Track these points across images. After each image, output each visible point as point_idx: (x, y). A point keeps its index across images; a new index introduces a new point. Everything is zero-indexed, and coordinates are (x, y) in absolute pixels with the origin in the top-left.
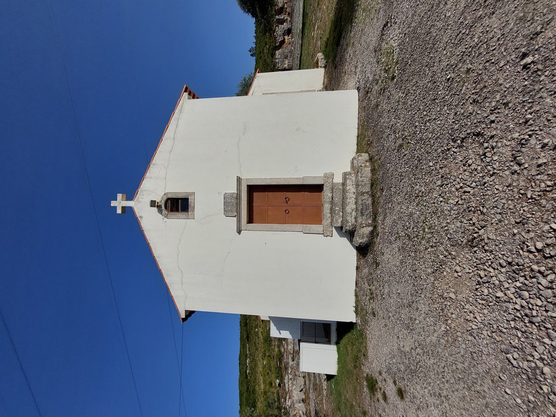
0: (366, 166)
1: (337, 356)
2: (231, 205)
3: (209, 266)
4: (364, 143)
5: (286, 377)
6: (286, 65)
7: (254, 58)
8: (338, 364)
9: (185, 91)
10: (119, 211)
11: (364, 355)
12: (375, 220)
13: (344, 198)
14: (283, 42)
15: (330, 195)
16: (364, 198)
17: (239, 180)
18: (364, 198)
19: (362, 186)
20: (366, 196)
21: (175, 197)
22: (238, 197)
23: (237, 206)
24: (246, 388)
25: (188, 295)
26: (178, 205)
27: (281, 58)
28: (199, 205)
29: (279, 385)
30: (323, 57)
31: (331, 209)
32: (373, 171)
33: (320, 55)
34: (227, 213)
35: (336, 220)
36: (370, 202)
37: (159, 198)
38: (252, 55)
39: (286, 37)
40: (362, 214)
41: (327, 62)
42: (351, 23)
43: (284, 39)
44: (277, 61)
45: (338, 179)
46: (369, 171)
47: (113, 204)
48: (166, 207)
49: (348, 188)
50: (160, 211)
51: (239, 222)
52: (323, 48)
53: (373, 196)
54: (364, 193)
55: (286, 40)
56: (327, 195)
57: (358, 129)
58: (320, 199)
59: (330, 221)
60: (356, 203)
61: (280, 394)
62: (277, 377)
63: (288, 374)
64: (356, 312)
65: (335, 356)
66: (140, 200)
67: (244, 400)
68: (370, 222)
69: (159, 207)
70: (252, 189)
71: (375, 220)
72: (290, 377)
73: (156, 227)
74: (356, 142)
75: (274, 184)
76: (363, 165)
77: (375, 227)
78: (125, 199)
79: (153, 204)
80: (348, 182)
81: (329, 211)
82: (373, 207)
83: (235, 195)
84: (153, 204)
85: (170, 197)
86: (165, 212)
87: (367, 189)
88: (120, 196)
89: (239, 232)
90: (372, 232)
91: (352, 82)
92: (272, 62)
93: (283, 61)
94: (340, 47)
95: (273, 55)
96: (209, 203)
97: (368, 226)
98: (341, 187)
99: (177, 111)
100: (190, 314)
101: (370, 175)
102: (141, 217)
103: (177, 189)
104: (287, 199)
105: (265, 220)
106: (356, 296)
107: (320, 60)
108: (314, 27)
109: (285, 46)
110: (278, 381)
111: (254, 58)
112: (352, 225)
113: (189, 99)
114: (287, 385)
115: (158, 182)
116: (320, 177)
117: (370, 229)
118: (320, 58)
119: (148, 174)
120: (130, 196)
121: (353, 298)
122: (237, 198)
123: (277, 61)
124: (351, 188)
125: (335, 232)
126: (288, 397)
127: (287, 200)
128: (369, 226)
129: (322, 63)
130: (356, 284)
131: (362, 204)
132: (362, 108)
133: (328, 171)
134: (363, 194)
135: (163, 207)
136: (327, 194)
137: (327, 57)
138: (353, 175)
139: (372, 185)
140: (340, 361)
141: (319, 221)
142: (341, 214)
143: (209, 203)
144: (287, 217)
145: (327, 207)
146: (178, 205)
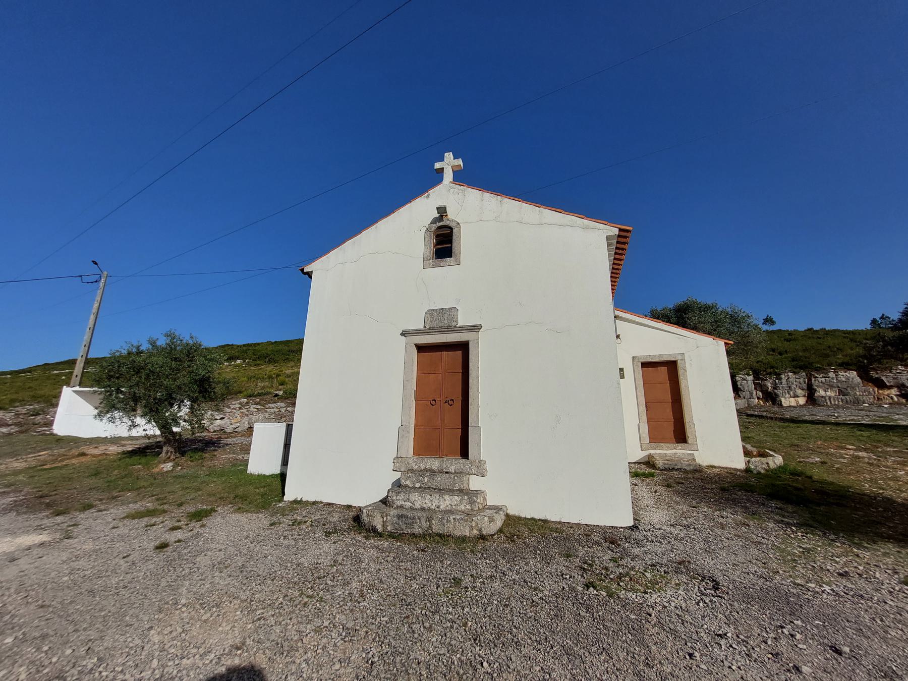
0: (472, 528)
1: (267, 474)
2: (441, 319)
3: (364, 296)
4: (514, 527)
5: (283, 405)
6: (821, 392)
7: (869, 327)
8: (259, 475)
9: (620, 230)
10: (437, 165)
11: (240, 508)
12: (391, 535)
13: (440, 491)
14: (881, 385)
15: (452, 469)
16: (423, 521)
17: (476, 328)
18: (423, 521)
19: (441, 520)
20: (426, 525)
21: (454, 237)
22: (451, 329)
23: (438, 328)
24: (293, 349)
25: (332, 273)
26: (444, 243)
27: (838, 381)
28: (446, 271)
29: (276, 395)
30: (772, 466)
31: (431, 470)
32: (463, 539)
33: (776, 460)
34: (430, 313)
35: (409, 477)
36: (417, 530)
37: (452, 215)
38: (874, 322)
39: (894, 392)
40: (400, 517)
41: (759, 473)
42: (799, 525)
43: (890, 387)
44: (831, 374)
45: (475, 483)
46: (464, 534)
47: (449, 156)
48: (440, 228)
49: (447, 497)
50: (434, 221)
51: (417, 332)
52: (792, 465)
53: (423, 536)
54: (430, 522)
55: (886, 392)
56: (451, 465)
57: (560, 523)
58: (450, 453)
59: (415, 467)
60: (423, 509)
61: (265, 397)
62: (285, 392)
63: (287, 407)
64: (295, 502)
65: (268, 472)
66: (452, 191)
67: (280, 347)
68: (389, 528)
69: (441, 218)
70: (464, 347)
71: (391, 535)
72: (283, 410)
73: (412, 220)
74: (537, 517)
75: (470, 381)
76: (474, 524)
77: (380, 535)
78: (455, 169)
79: (442, 211)
80: (456, 498)
81: (428, 467)
82: (410, 535)
83: (454, 324)
84: (442, 211)
85: (454, 231)
86: (434, 227)
87: (436, 528)
88: (460, 162)
89: (403, 334)
90: (374, 530)
91: (658, 517)
92: (830, 365)
93: (831, 387)
94: (760, 499)
95: (846, 366)
96: (446, 286)
97: (384, 524)
98: (457, 487)
99: (586, 222)
100: (310, 275)
101: (457, 533)
102: (428, 196)
103: (464, 242)
104: (451, 402)
105: (422, 370)
106: (315, 503)
107: (764, 460)
108: (865, 450)
109: (871, 388)
110: (281, 393)
111: (869, 327)
112: (393, 501)
113: (608, 238)
114: (273, 405)
115: (477, 212)
116: (480, 454)
117: (380, 528)
118: (770, 460)
119: (487, 195)
120: (460, 177)
121: (312, 499)
122: (449, 327)
123: (831, 374)
124: (447, 502)
125: (398, 475)
126: (259, 407)
127: (450, 402)
128: (383, 526)
129: (759, 464)
130: (329, 504)
131: (414, 518)
132: (587, 533)
133: (488, 467)
134: (429, 519)
135: (441, 224)
136: (454, 464)
137: (772, 475)
138: (468, 507)
139: (440, 536)
140: (262, 477)
141: (417, 452)
142: (418, 485)
143: (446, 286)
144: (426, 400)
145: (434, 463)
146: (444, 243)
